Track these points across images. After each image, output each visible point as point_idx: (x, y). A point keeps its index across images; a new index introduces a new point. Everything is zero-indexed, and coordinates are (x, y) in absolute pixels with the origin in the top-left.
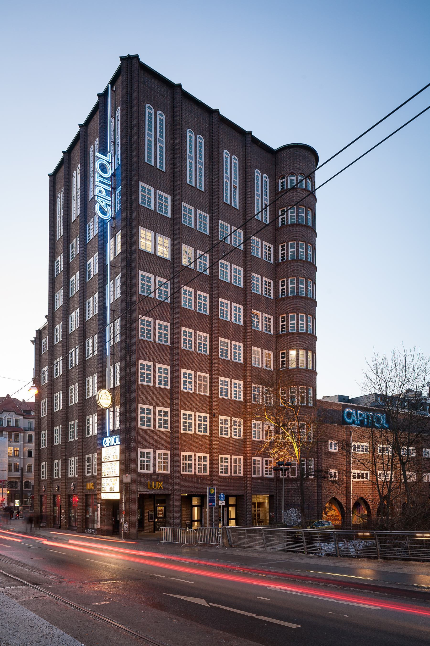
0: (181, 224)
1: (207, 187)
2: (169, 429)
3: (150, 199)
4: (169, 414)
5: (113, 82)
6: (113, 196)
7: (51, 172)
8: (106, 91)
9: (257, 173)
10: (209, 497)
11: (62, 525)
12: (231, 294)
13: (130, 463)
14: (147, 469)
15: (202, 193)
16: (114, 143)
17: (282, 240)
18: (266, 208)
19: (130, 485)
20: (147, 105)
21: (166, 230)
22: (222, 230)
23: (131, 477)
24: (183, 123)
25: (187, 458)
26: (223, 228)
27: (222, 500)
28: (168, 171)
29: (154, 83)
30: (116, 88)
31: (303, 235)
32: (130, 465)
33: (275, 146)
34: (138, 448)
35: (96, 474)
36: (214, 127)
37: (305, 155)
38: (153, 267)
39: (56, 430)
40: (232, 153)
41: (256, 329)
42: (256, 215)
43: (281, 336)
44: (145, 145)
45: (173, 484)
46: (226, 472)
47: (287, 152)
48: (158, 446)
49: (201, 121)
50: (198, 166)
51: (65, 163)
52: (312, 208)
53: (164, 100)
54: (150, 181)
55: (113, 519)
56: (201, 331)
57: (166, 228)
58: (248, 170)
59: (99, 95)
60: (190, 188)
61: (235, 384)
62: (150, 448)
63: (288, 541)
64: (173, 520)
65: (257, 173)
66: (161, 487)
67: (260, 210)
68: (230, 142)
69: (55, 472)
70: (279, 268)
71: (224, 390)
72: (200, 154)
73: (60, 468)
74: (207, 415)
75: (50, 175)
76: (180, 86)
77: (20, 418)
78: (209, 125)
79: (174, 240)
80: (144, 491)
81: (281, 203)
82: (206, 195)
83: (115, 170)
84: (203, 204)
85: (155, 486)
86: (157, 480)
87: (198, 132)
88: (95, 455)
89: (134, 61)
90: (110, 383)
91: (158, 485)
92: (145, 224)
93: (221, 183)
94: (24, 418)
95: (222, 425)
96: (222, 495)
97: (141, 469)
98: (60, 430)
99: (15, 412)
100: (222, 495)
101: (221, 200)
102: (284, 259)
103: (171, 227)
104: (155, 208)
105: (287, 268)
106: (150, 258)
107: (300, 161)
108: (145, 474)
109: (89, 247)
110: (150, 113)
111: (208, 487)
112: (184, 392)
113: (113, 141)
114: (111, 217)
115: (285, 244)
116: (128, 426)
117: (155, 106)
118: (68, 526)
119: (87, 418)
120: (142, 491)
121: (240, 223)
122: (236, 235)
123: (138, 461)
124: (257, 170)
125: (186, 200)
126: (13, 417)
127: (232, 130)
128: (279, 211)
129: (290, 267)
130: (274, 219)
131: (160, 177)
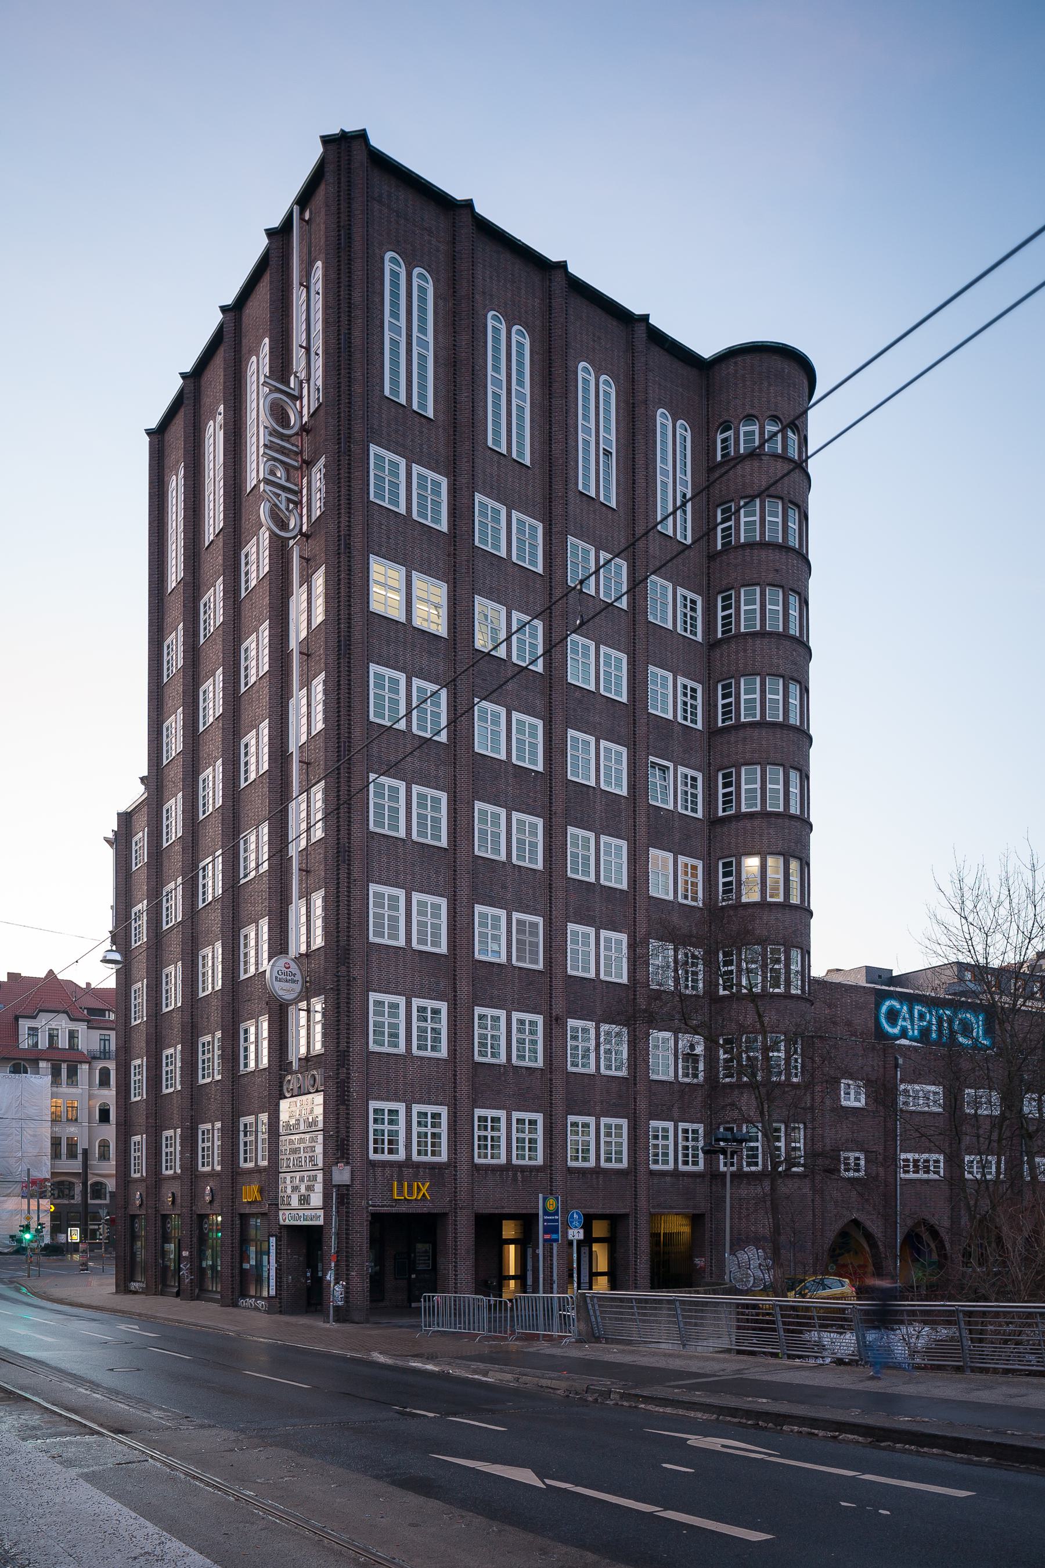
1: (536, 455)
2: (443, 1053)
5: (304, 199)
6: (305, 481)
7: (153, 424)
8: (288, 221)
9: (662, 418)
10: (545, 1221)
11: (182, 1287)
12: (597, 719)
13: (348, 1136)
15: (524, 470)
17: (724, 582)
19: (348, 1190)
20: (389, 255)
21: (437, 563)
23: (352, 1172)
27: (576, 1227)
28: (441, 417)
29: (403, 197)
30: (311, 213)
31: (777, 571)
32: (348, 1141)
33: (706, 350)
34: (367, 1101)
38: (404, 655)
40: (600, 369)
43: (723, 820)
45: (456, 1188)
47: (736, 363)
48: (417, 1096)
49: (523, 292)
51: (186, 402)
52: (800, 503)
53: (429, 242)
54: (397, 443)
55: (309, 1274)
59: (270, 233)
60: (496, 457)
63: (739, 1328)
64: (456, 1275)
65: (662, 418)
66: (424, 1195)
73: (178, 1148)
75: (149, 433)
76: (469, 205)
77: (81, 1028)
79: (455, 587)
80: (383, 1206)
81: (721, 491)
85: (410, 1193)
86: (416, 1177)
87: (515, 319)
89: (357, 145)
92: (384, 550)
93: (571, 443)
94: (89, 1028)
97: (376, 1151)
98: (179, 1057)
99: (66, 1012)
101: (571, 486)
102: (730, 630)
103: (449, 555)
105: (737, 652)
107: (770, 385)
108: (384, 1164)
109: (246, 607)
110: (395, 275)
115: (733, 592)
116: (343, 1046)
119: (243, 1026)
120: (379, 1206)
123: (368, 1131)
126: (64, 1025)
129: (745, 651)
130: (705, 531)
131: (421, 432)
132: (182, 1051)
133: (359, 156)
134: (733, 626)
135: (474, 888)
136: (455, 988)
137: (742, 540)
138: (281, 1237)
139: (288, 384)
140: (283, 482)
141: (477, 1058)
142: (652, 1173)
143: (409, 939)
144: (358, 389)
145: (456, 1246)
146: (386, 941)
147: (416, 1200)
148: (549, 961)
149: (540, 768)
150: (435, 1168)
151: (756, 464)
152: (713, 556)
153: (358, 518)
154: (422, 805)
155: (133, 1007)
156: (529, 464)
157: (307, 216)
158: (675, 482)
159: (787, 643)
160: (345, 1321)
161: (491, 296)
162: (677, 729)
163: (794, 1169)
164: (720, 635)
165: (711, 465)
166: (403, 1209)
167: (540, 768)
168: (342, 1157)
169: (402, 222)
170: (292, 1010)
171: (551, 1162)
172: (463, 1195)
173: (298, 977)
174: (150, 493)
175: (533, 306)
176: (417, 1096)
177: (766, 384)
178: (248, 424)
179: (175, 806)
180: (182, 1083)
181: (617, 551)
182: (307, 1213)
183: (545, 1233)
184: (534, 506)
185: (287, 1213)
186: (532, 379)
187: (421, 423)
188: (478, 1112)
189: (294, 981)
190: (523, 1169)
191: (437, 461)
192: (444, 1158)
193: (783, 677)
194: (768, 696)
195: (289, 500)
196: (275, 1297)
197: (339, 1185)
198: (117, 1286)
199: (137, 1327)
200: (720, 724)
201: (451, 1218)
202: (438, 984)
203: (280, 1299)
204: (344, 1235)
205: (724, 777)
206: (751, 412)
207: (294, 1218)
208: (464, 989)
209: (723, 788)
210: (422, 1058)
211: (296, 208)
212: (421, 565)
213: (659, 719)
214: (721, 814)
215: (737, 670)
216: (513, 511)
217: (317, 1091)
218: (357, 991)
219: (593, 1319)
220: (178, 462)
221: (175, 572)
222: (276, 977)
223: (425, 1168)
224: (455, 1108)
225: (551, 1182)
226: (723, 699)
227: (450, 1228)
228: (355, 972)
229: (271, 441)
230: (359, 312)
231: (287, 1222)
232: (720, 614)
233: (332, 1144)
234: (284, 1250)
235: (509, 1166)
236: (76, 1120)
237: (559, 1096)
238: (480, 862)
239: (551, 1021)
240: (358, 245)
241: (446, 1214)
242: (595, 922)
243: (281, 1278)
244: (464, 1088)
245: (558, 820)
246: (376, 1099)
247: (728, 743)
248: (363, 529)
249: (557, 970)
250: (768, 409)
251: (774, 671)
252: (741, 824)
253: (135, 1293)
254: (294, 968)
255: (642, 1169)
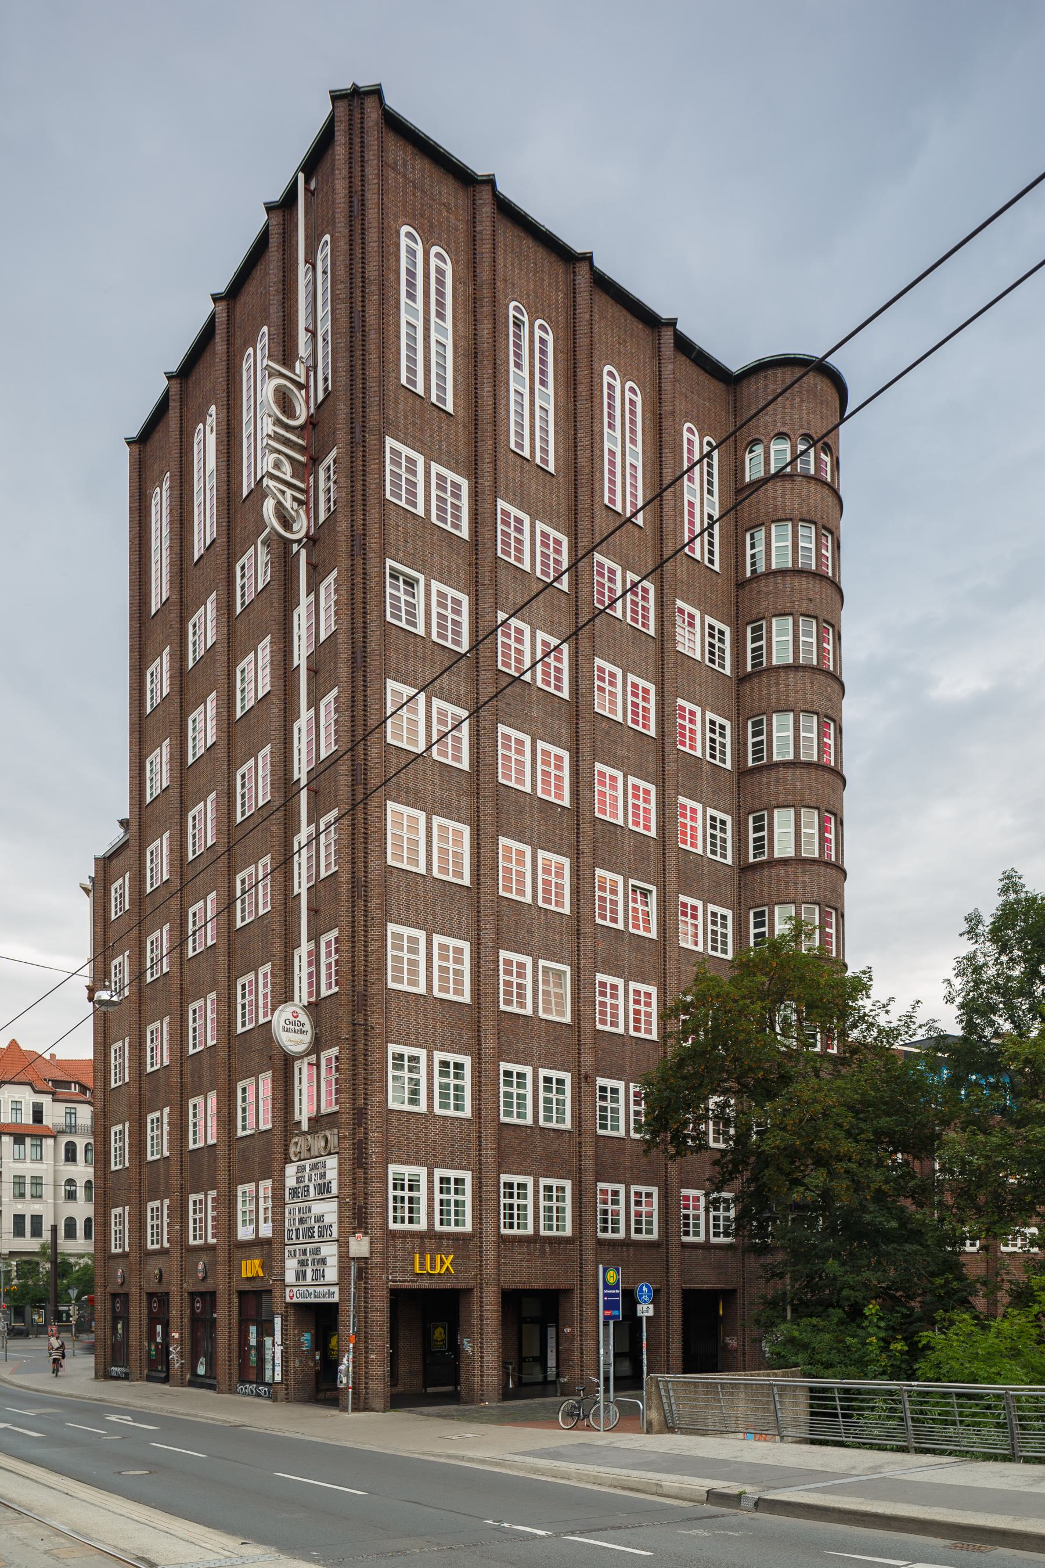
0: (497, 558)
1: (561, 462)
2: (467, 1113)
3: (414, 485)
4: (467, 1071)
5: (312, 164)
6: (311, 479)
7: (134, 432)
8: (291, 194)
10: (605, 1295)
11: (172, 1372)
12: (625, 752)
13: (366, 1203)
14: (411, 1221)
15: (548, 477)
16: (314, 334)
17: (755, 612)
18: (711, 526)
19: (366, 1263)
20: (405, 229)
21: (458, 573)
22: (601, 580)
23: (371, 1243)
24: (498, 284)
25: (515, 1191)
26: (602, 575)
27: (645, 1302)
28: (461, 413)
29: (420, 168)
30: (317, 183)
31: (810, 600)
32: (366, 1208)
33: (735, 365)
34: (387, 1164)
35: (214, 1241)
36: (578, 299)
37: (816, 385)
39: (152, 1121)
40: (625, 375)
41: (688, 847)
42: (688, 544)
43: (754, 867)
44: (398, 338)
45: (481, 1261)
46: (615, 1230)
47: (766, 377)
48: (440, 1159)
49: (546, 283)
50: (538, 402)
51: (172, 404)
52: (834, 530)
53: (448, 219)
54: (414, 437)
55: (317, 1357)
56: (549, 851)
57: (457, 566)
58: (667, 423)
59: (270, 208)
60: (519, 461)
61: (637, 992)
62: (418, 1163)
63: (812, 1414)
64: (482, 1357)
66: (448, 1268)
67: (697, 530)
68: (619, 344)
69: (152, 1234)
70: (747, 687)
71: (609, 1010)
72: (633, 431)
73: (166, 1220)
74: (567, 1076)
76: (490, 182)
77: (46, 1100)
78: (566, 294)
79: (477, 600)
80: (404, 1281)
81: (750, 514)
82: (558, 483)
83: (318, 407)
84: (551, 506)
85: (433, 1267)
86: (438, 1250)
87: (537, 312)
88: (266, 1184)
89: (370, 103)
90: (302, 994)
91: (442, 1262)
92: (401, 554)
93: (597, 452)
94: (54, 1100)
95: (603, 1104)
96: (645, 1289)
97: (395, 1220)
98: (166, 1120)
99: (30, 1084)
100: (645, 1289)
101: (597, 498)
102: (761, 663)
103: (470, 565)
104: (428, 510)
105: (769, 686)
106: (415, 645)
107: (802, 401)
108: (405, 1235)
109: (241, 627)
110: (412, 253)
111: (601, 1267)
112: (505, 1012)
113: (310, 328)
114: (307, 535)
115: (764, 622)
117: (424, 233)
118: (188, 1376)
119: (240, 1085)
120: (399, 1281)
121: (646, 563)
122: (636, 594)
123: (387, 1198)
124: (688, 425)
125: (507, 493)
126: (27, 1097)
127: (625, 312)
128: (744, 537)
129: (778, 684)
131: (440, 428)
132: (170, 1115)
133: (373, 116)
134: (764, 659)
135: (498, 932)
136: (479, 1040)
137: (774, 567)
138: (287, 1316)
139: (293, 371)
140: (288, 478)
141: (503, 1119)
142: (685, 1246)
143: (430, 986)
144: (372, 372)
145: (482, 1325)
146: (405, 987)
147: (439, 1274)
148: (577, 1013)
149: (566, 802)
150: (459, 1240)
151: (788, 485)
152: (741, 584)
153: (374, 515)
154: (443, 838)
155: (113, 1067)
156: (553, 472)
157: (313, 186)
158: (702, 503)
159: (822, 678)
160: (365, 1409)
161: (513, 285)
162: (706, 768)
163: (253, 1329)
164: (749, 669)
165: (739, 486)
166: (425, 1284)
167: (566, 802)
168: (360, 1226)
169: (419, 194)
170: (297, 1064)
171: (581, 1233)
172: (490, 1269)
173: (308, 1027)
174: (130, 508)
175: (557, 300)
176: (440, 1159)
177: (798, 400)
178: (244, 422)
179: (160, 848)
180: (170, 1149)
181: (644, 574)
182: (318, 1289)
183: (605, 1309)
184: (559, 518)
185: (295, 1289)
186: (555, 380)
187: (440, 418)
188: (505, 1178)
189: (303, 1032)
190: (550, 1240)
191: (457, 460)
192: (468, 1228)
193: (817, 714)
194: (802, 734)
195: (295, 499)
196: (282, 1382)
197: (358, 1258)
198: (96, 1374)
199: (129, 1418)
200: (750, 764)
201: (476, 1294)
202: (461, 1035)
203: (287, 1385)
204: (363, 1314)
205: (755, 820)
206: (784, 430)
207: (303, 1295)
208: (489, 1041)
209: (754, 832)
210: (445, 1117)
211: (301, 177)
212: (441, 574)
213: (687, 757)
214: (751, 860)
215: (769, 706)
216: (537, 522)
217: (330, 1154)
218: (374, 1041)
219: (666, 1407)
220: (162, 473)
221: (160, 591)
222: (284, 1027)
223: (448, 1239)
224: (480, 1173)
225: (581, 1255)
226: (753, 737)
227: (476, 1306)
228: (375, 1021)
229: (275, 432)
230: (374, 288)
231: (295, 1300)
232: (750, 646)
233: (348, 1212)
234: (291, 1331)
235: (536, 1238)
236: (41, 1197)
237: (588, 1162)
238: (505, 903)
239: (579, 1079)
240: (372, 213)
241: (470, 1290)
242: (623, 972)
243: (287, 1362)
244: (490, 1151)
245: (586, 860)
246: (395, 1162)
247: (760, 783)
248: (380, 528)
249: (585, 1024)
250: (801, 427)
251: (808, 707)
252: (774, 871)
253: (117, 1378)
254: (303, 1018)
255: (673, 1241)
